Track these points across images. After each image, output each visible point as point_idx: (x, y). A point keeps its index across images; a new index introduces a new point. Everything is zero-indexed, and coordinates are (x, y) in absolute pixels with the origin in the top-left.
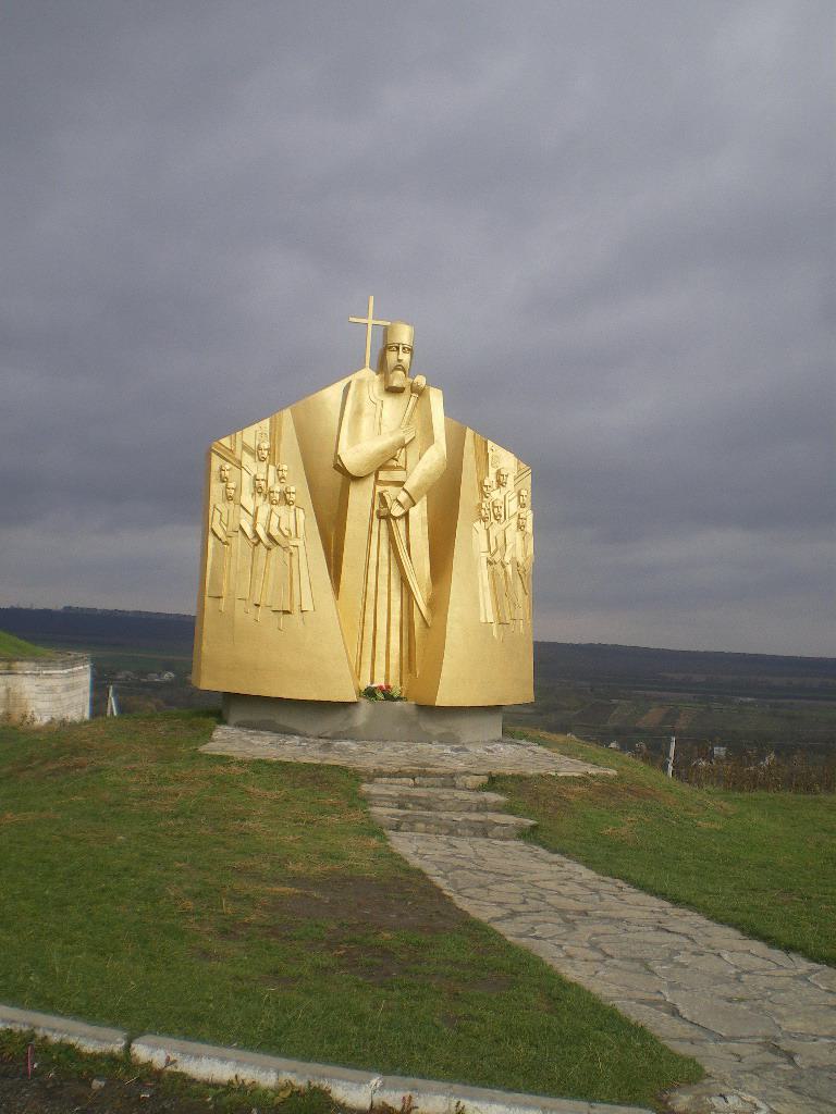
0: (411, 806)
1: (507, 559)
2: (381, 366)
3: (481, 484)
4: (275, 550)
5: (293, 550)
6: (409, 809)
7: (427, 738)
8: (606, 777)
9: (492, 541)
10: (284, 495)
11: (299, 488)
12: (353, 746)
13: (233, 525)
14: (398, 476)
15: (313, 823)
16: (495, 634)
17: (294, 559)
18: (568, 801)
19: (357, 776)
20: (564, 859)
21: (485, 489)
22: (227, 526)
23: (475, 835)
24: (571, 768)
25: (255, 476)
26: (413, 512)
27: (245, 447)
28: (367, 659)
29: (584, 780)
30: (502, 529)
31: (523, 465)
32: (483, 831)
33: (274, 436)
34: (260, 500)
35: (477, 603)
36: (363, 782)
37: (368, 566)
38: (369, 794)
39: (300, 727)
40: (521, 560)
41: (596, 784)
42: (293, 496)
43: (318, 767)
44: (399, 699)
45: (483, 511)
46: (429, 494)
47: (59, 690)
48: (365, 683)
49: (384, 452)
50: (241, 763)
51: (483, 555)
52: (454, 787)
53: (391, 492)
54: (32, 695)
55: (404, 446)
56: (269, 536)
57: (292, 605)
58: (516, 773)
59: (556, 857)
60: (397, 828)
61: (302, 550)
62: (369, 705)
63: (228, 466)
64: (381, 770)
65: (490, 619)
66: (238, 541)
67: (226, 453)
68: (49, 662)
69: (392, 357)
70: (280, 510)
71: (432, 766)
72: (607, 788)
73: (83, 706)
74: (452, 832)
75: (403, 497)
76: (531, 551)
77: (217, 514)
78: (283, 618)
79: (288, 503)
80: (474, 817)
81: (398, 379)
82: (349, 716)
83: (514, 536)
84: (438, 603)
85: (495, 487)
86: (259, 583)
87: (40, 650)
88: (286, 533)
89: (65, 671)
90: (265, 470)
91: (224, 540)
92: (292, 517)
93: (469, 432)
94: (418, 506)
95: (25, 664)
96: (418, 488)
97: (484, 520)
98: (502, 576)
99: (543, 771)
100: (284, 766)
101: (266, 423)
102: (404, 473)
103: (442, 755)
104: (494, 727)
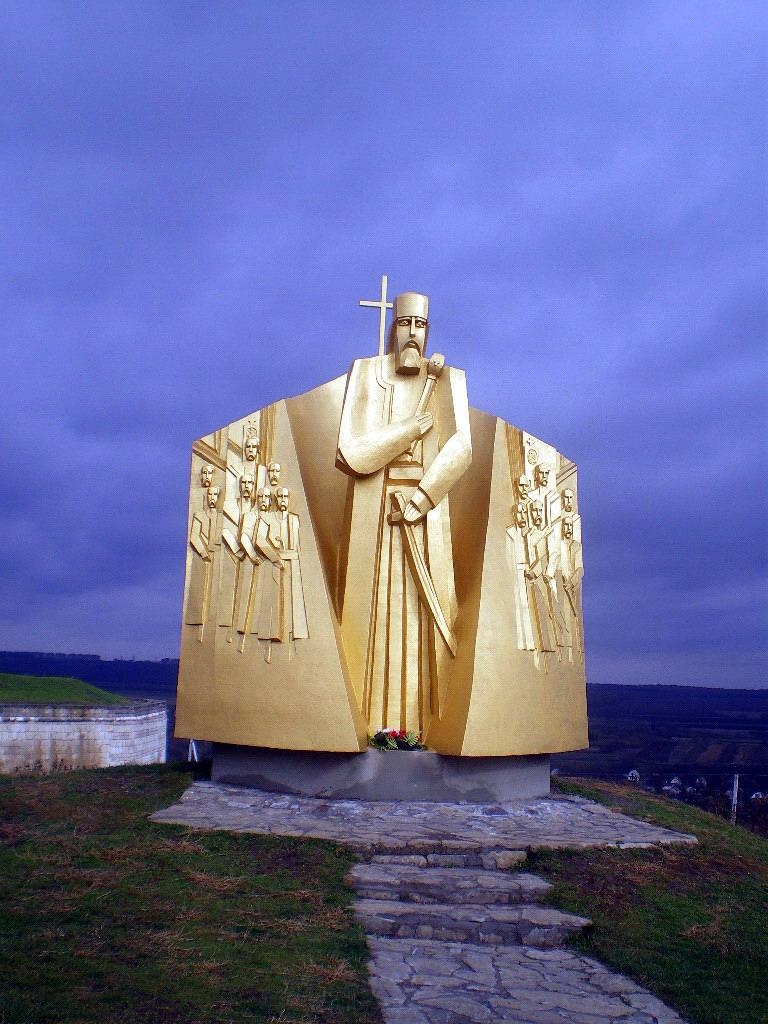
0: (417, 897)
1: (551, 573)
2: (392, 346)
3: (516, 483)
4: (263, 564)
5: (285, 564)
6: (414, 901)
7: (453, 797)
8: (681, 849)
9: (531, 550)
11: (292, 491)
12: (355, 809)
14: (412, 473)
15: (261, 932)
18: (632, 883)
19: (349, 854)
20: (630, 986)
21: (521, 489)
22: (209, 538)
23: (504, 943)
24: (638, 836)
25: (241, 478)
26: (432, 516)
27: (231, 445)
28: (378, 699)
29: (655, 853)
30: (543, 540)
32: (516, 935)
33: (265, 428)
35: (513, 624)
36: (357, 861)
37: (377, 583)
38: (358, 881)
39: (295, 787)
40: (567, 573)
41: (673, 858)
42: (286, 500)
43: (297, 841)
44: (416, 747)
45: (519, 515)
46: (452, 494)
47: (133, 735)
48: (376, 727)
49: (395, 444)
50: (196, 836)
51: (519, 567)
52: (481, 866)
53: (404, 493)
54: (107, 741)
55: (420, 437)
56: (257, 549)
57: (282, 632)
58: (564, 845)
59: (620, 982)
60: (392, 934)
61: (295, 564)
62: (380, 756)
63: (210, 468)
64: (381, 845)
65: (531, 645)
66: (221, 555)
67: (208, 452)
68: (124, 710)
69: (403, 332)
70: (270, 517)
71: (454, 837)
72: (686, 863)
73: (159, 752)
74: (471, 938)
75: (418, 498)
76: (579, 563)
77: (197, 524)
78: (271, 647)
79: (280, 509)
80: (504, 914)
81: (411, 359)
83: (558, 545)
84: (464, 627)
85: (533, 488)
86: (244, 606)
87: (116, 697)
88: (277, 544)
89: (139, 718)
90: (253, 471)
91: (205, 555)
94: (438, 507)
95: (99, 711)
96: (437, 487)
97: (521, 525)
98: (544, 594)
99: (599, 843)
100: (252, 841)
101: (257, 415)
102: (420, 469)
103: (469, 819)
104: (540, 781)
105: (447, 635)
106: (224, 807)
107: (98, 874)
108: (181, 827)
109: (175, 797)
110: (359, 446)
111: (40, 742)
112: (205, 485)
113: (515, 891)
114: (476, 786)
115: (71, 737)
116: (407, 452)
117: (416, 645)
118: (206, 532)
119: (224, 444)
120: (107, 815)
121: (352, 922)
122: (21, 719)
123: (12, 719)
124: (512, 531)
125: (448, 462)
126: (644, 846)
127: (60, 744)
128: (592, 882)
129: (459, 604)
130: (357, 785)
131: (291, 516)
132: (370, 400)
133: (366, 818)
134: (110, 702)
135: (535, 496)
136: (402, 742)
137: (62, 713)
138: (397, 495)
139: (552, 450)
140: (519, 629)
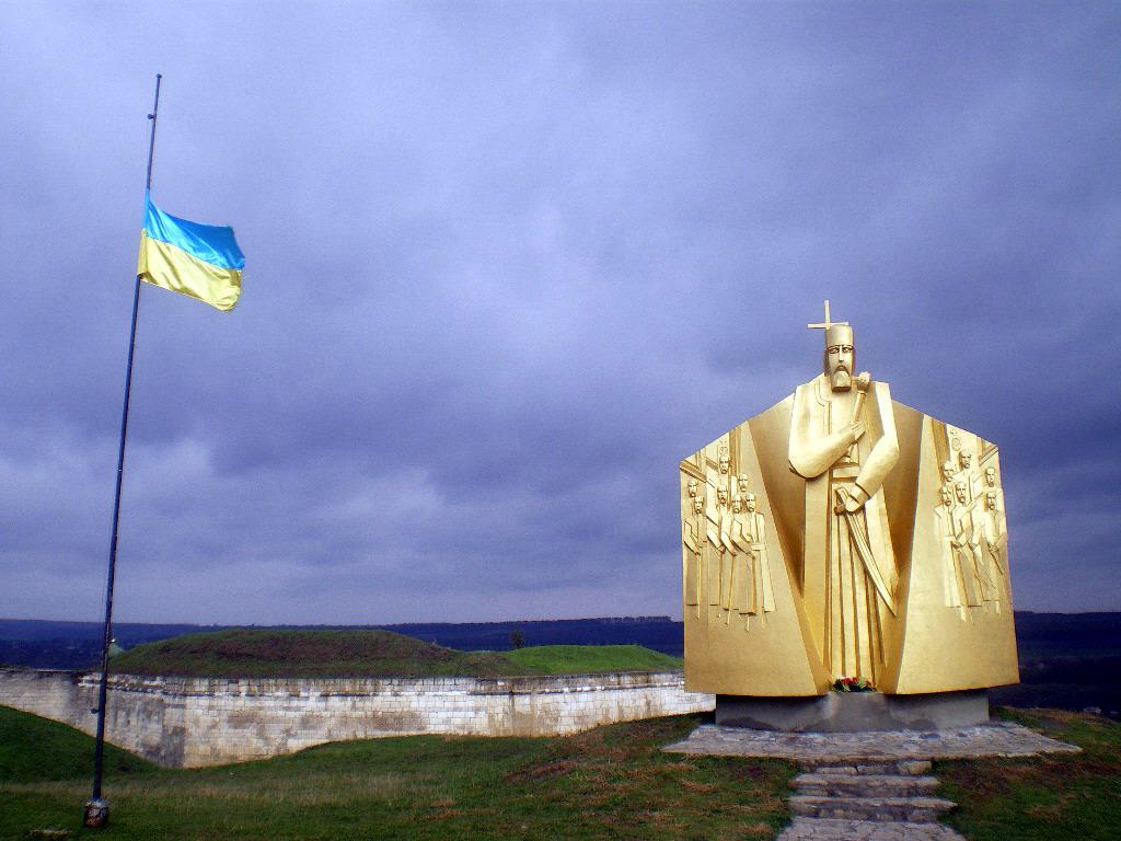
0: (840, 793)
1: (975, 540)
3: (942, 469)
4: (740, 555)
7: (899, 726)
10: (744, 502)
11: (757, 495)
12: (818, 738)
13: (702, 537)
14: (851, 471)
16: (963, 617)
17: (757, 561)
19: (797, 767)
21: (946, 473)
26: (869, 505)
28: (837, 653)
31: (988, 444)
32: (902, 814)
33: (733, 450)
34: (724, 509)
35: (940, 586)
39: (775, 724)
40: (991, 539)
43: (761, 760)
44: (867, 689)
45: (945, 496)
48: (837, 675)
49: (834, 451)
50: (692, 759)
55: (856, 442)
56: (734, 544)
57: (755, 606)
58: (961, 756)
61: (763, 553)
63: (694, 481)
65: (957, 602)
70: (741, 517)
75: (856, 492)
76: (1003, 528)
77: (688, 527)
81: (843, 379)
82: (819, 709)
84: (900, 594)
88: (748, 539)
91: (696, 550)
92: (753, 521)
93: (927, 419)
94: (874, 498)
95: (663, 676)
96: (870, 481)
97: (947, 503)
98: (970, 559)
104: (981, 710)
105: (888, 599)
106: (721, 741)
107: (619, 785)
108: (682, 755)
109: (685, 736)
110: (805, 451)
111: (607, 710)
112: (692, 495)
113: (913, 788)
114: (918, 718)
115: (637, 703)
116: (845, 455)
117: (864, 609)
118: (695, 532)
119: (703, 461)
120: (633, 751)
121: (786, 807)
122: (587, 688)
123: (579, 689)
124: (939, 510)
125: (879, 461)
126: (1029, 755)
127: (626, 710)
128: (974, 780)
129: (899, 575)
130: (823, 722)
131: (758, 516)
132: (812, 418)
133: (824, 744)
134: (672, 666)
135: (959, 478)
136: (854, 686)
137: (626, 680)
138: (839, 491)
139: (973, 436)
140: (947, 591)
